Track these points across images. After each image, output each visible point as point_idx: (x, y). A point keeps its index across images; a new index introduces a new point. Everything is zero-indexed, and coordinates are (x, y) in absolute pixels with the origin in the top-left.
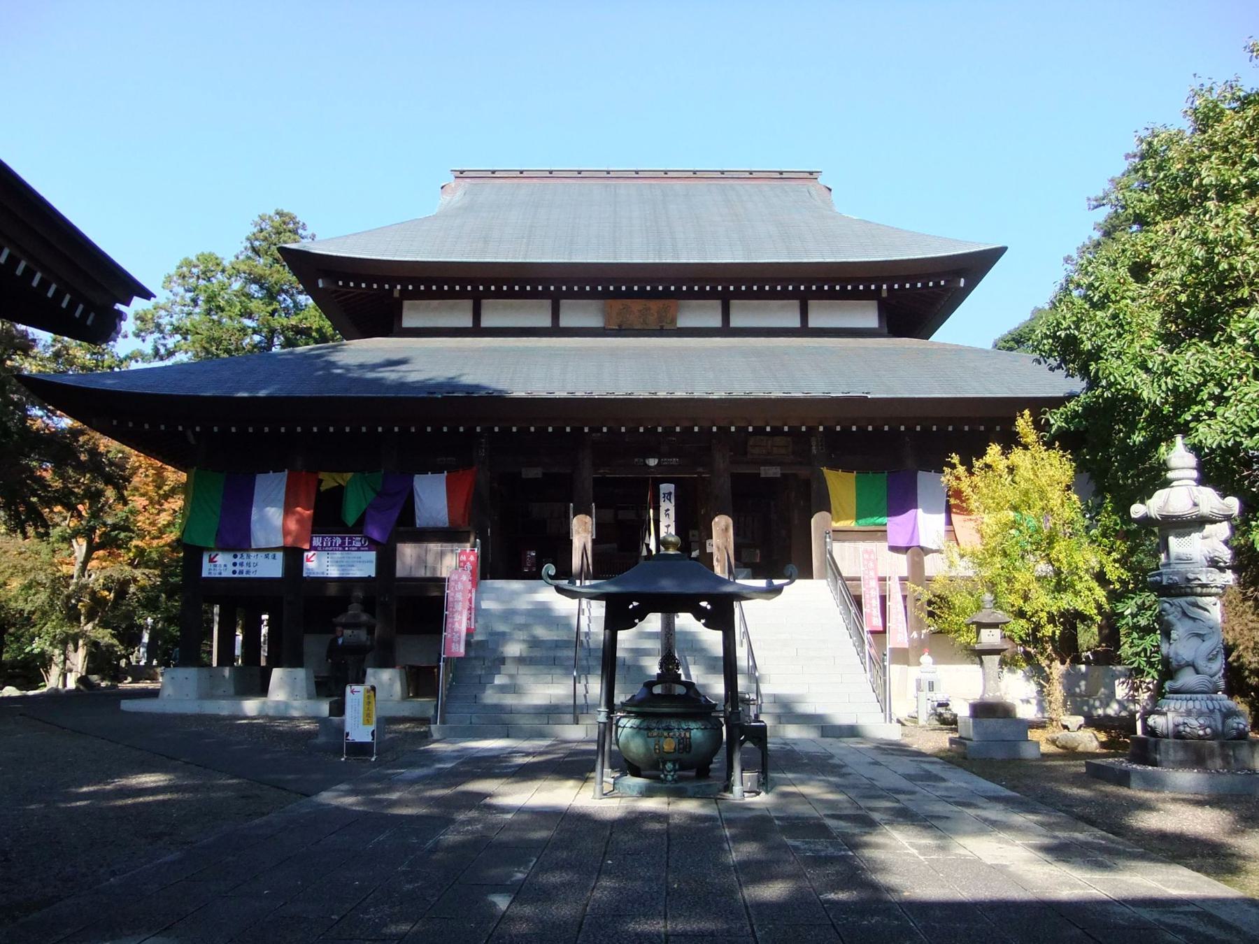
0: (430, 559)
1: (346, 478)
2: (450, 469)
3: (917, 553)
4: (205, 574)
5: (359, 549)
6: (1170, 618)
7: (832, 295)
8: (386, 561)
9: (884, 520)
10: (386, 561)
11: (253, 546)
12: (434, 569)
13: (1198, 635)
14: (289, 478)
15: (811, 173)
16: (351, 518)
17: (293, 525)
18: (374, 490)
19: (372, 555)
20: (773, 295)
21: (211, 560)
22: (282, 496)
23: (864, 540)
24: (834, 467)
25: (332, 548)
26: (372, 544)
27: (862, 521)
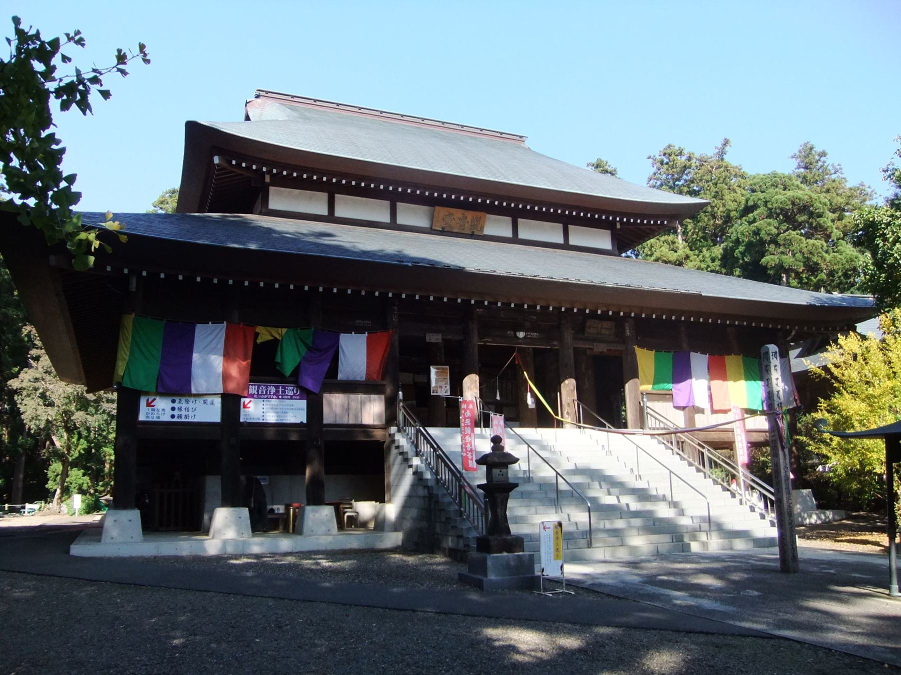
0: (353, 405)
1: (279, 333)
2: (371, 331)
3: (692, 410)
4: (142, 417)
5: (291, 398)
8: (315, 410)
9: (670, 386)
10: (315, 410)
11: (194, 391)
12: (356, 417)
14: (227, 328)
15: (521, 137)
16: (288, 370)
17: (234, 371)
18: (306, 345)
19: (303, 404)
21: (149, 405)
22: (221, 345)
23: (658, 401)
24: (641, 346)
25: (266, 396)
26: (305, 393)
27: (656, 386)
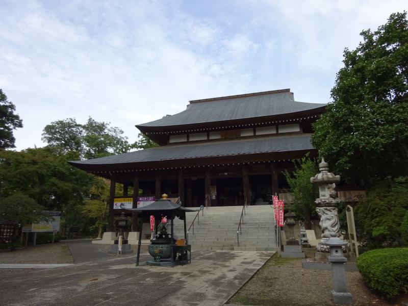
6: (320, 214)
7: (285, 123)
13: (328, 219)
20: (268, 125)
